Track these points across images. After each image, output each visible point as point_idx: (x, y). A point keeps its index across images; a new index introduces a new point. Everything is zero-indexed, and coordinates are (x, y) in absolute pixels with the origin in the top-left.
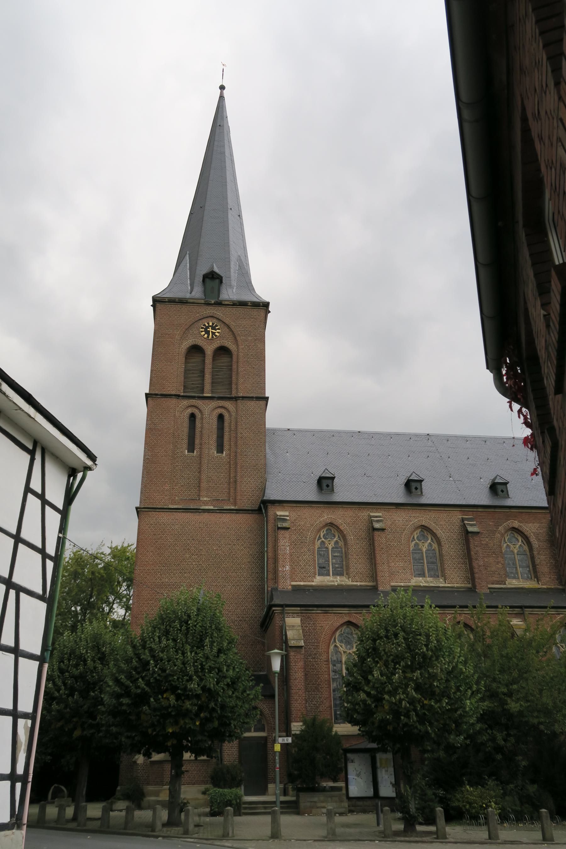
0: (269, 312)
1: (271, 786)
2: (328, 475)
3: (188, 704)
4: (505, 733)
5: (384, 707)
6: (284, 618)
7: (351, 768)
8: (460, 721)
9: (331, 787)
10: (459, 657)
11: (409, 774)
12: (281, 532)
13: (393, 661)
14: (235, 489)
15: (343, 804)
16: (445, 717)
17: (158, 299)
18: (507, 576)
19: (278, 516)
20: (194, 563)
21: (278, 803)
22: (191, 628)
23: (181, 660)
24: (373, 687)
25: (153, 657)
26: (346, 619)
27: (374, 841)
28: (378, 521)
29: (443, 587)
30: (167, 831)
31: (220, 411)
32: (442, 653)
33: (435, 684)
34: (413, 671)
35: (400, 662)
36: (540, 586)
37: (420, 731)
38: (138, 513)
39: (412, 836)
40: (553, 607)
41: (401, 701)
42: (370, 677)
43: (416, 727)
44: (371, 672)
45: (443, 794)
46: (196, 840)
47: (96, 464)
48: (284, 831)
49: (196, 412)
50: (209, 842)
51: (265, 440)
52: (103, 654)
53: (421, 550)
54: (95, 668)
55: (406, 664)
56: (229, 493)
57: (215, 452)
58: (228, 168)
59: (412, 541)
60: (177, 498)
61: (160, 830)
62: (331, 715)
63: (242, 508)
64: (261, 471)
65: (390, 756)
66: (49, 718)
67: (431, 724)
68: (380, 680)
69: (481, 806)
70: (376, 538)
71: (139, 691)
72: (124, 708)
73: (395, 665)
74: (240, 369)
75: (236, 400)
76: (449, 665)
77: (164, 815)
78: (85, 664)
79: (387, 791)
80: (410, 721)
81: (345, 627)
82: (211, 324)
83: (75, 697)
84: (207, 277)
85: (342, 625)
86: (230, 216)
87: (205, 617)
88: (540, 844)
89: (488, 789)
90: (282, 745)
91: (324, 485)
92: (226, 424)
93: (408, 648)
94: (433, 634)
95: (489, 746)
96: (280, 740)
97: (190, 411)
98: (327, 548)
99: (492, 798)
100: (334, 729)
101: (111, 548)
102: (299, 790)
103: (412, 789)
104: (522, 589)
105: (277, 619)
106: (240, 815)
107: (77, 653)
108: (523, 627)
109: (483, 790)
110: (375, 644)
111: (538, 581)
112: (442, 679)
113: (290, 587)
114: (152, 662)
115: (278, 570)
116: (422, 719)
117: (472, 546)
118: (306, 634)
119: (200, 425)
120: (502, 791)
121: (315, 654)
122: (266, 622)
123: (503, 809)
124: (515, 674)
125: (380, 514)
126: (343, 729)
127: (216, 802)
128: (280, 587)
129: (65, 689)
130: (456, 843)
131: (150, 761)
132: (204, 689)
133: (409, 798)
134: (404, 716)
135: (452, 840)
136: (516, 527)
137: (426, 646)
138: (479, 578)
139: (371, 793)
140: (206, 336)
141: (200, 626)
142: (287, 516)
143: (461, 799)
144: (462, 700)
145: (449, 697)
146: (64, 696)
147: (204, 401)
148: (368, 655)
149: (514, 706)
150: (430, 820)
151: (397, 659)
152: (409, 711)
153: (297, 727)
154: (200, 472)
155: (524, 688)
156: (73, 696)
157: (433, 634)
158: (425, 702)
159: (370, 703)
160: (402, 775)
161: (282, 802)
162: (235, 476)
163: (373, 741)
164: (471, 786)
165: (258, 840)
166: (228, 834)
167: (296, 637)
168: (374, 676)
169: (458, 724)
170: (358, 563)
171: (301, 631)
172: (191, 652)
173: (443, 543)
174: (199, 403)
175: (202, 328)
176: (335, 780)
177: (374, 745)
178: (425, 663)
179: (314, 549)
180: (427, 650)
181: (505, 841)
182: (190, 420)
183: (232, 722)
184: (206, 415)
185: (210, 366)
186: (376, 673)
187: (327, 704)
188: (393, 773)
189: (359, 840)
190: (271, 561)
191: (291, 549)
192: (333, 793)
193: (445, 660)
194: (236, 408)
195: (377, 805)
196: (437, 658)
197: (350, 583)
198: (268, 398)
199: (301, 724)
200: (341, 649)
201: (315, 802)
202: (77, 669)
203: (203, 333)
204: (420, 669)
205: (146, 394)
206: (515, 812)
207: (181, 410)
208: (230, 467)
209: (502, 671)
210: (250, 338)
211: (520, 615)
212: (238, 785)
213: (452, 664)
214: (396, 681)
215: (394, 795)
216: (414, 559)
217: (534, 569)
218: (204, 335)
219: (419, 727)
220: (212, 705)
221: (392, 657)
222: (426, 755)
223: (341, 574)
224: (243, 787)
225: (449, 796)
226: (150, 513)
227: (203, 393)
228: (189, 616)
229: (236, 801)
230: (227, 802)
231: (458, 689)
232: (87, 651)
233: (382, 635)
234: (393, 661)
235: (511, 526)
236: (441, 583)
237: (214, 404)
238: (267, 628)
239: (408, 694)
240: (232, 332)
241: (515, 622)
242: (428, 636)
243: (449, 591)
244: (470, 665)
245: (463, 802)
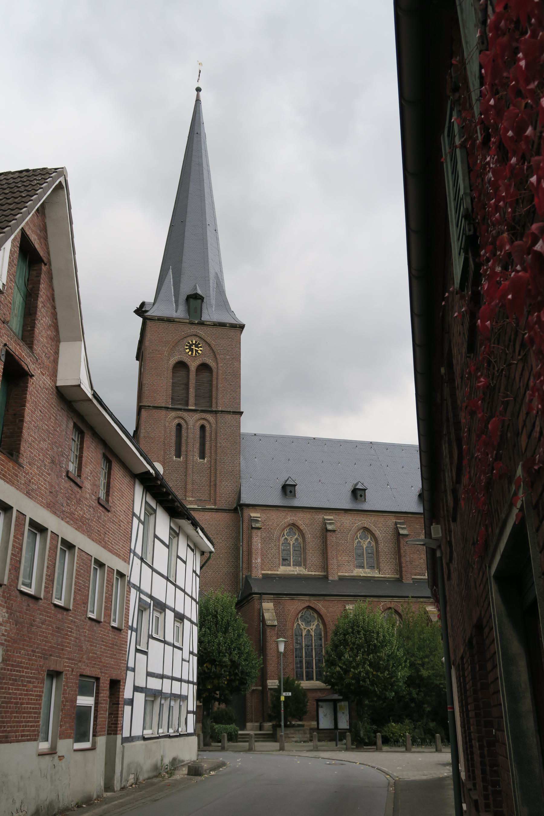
1: (249, 725)
6: (261, 603)
19: (251, 517)
24: (344, 664)
26: (307, 604)
28: (330, 524)
29: (377, 577)
31: (202, 422)
34: (368, 655)
41: (360, 672)
49: (182, 422)
53: (362, 547)
55: (365, 650)
58: (206, 181)
63: (221, 508)
64: (236, 476)
69: (400, 735)
79: (344, 724)
81: (305, 610)
82: (194, 342)
84: (191, 298)
85: (304, 609)
90: (286, 697)
92: (207, 434)
96: (284, 694)
97: (177, 421)
99: (407, 730)
106: (237, 742)
108: (435, 613)
109: (402, 725)
113: (261, 576)
115: (251, 561)
116: (373, 683)
117: (402, 545)
118: (279, 615)
119: (185, 434)
121: (284, 630)
125: (332, 517)
128: (253, 575)
132: (231, 660)
137: (377, 639)
139: (332, 727)
140: (190, 353)
142: (259, 518)
145: (389, 671)
148: (341, 643)
149: (425, 673)
151: (359, 647)
154: (186, 476)
155: (432, 661)
162: (215, 480)
164: (394, 722)
167: (271, 618)
169: (392, 685)
170: (313, 557)
174: (185, 415)
175: (187, 346)
178: (375, 650)
182: (177, 429)
184: (191, 426)
185: (194, 381)
186: (347, 656)
187: (291, 667)
190: (245, 553)
192: (299, 728)
197: (306, 572)
198: (241, 413)
200: (302, 627)
203: (188, 350)
204: (372, 653)
206: (421, 739)
208: (211, 472)
209: (420, 649)
210: (228, 357)
218: (188, 352)
223: (300, 565)
227: (187, 405)
228: (216, 611)
234: (356, 648)
236: (376, 574)
237: (197, 416)
240: (213, 350)
242: (378, 633)
243: (382, 580)
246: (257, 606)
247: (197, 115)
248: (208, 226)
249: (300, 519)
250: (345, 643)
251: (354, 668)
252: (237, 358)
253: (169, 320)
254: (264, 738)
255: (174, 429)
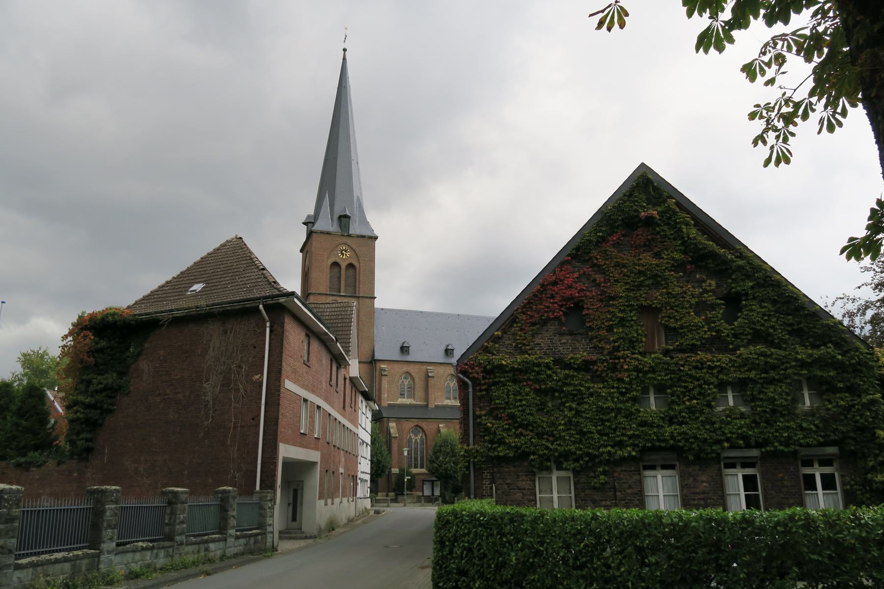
1: (380, 494)
9: (47, 560)
65: (439, 483)
79: (437, 493)
118: (399, 430)
151: (448, 454)
170: (419, 393)
227: (340, 292)
246: (386, 425)
249: (411, 369)
250: (440, 451)
252: (372, 260)
253: (328, 233)
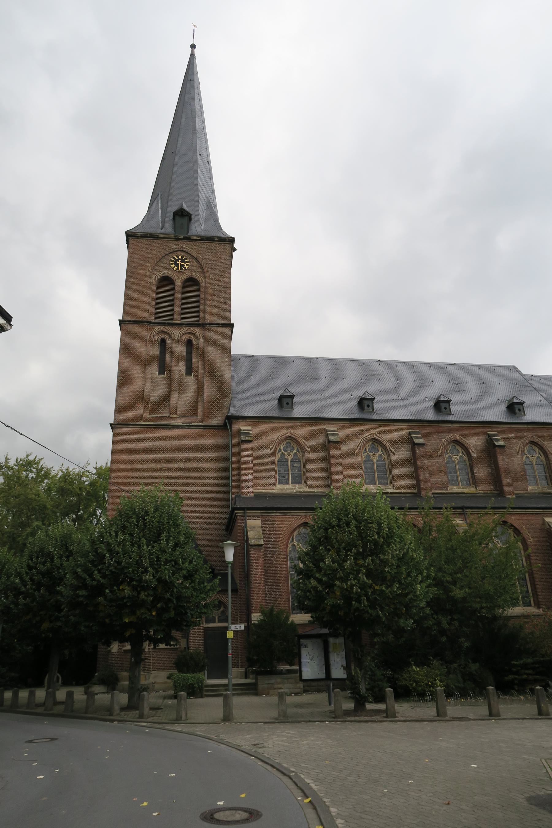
0: (235, 250)
2: (287, 394)
3: (143, 595)
4: (449, 617)
5: (335, 593)
7: (305, 653)
8: (410, 605)
9: (288, 670)
10: (410, 544)
11: (360, 657)
12: (245, 445)
13: (344, 549)
14: (203, 407)
15: (298, 685)
16: (396, 601)
17: (131, 233)
18: (448, 482)
20: (164, 474)
21: (231, 687)
22: (148, 524)
23: (137, 553)
24: (325, 575)
25: (110, 551)
26: (303, 520)
27: (325, 721)
28: (333, 435)
30: (125, 715)
31: (188, 336)
32: (393, 541)
33: (387, 570)
34: (364, 558)
35: (352, 549)
36: (478, 491)
37: (371, 615)
38: (112, 428)
39: (361, 716)
40: (492, 508)
41: (352, 586)
42: (322, 564)
43: (367, 612)
44: (323, 560)
45: (391, 674)
46: (148, 724)
47: (11, 325)
48: (236, 713)
50: (161, 726)
51: (230, 363)
52: (71, 552)
53: (372, 460)
54: (62, 565)
55: (358, 551)
56: (197, 411)
57: (184, 374)
59: (364, 453)
60: (148, 416)
61: (118, 714)
62: (289, 607)
65: (340, 640)
66: (16, 611)
67: (382, 609)
68: (331, 567)
69: (427, 684)
70: (332, 450)
71: (95, 583)
72: (81, 599)
73: (346, 553)
74: (207, 299)
75: (204, 327)
76: (400, 552)
77: (123, 698)
78: (52, 561)
79: (338, 672)
80: (361, 605)
82: (180, 257)
83: (41, 592)
84: (177, 215)
85: (299, 526)
86: (199, 161)
87: (162, 513)
88: (487, 719)
89: (433, 669)
91: (285, 404)
92: (194, 349)
93: (360, 536)
94: (385, 522)
95: (435, 630)
96: (233, 627)
97: (160, 336)
98: (287, 459)
99: (437, 676)
100: (291, 619)
101: (96, 468)
102: (258, 673)
103: (363, 671)
104: (462, 494)
105: (239, 522)
106: (202, 697)
107: (46, 550)
109: (429, 669)
110: (327, 533)
111: (476, 487)
112: (393, 565)
113: (252, 494)
114: (107, 555)
116: (373, 604)
117: (418, 456)
119: (170, 349)
120: (446, 670)
122: (230, 527)
123: (447, 686)
124: (460, 564)
125: (335, 429)
126: (301, 618)
127: (179, 686)
128: (243, 494)
129: (31, 584)
130: (405, 721)
131: (124, 650)
132: (159, 580)
133: (360, 680)
134: (356, 601)
135: (402, 719)
136: (458, 439)
137: (378, 533)
138: (424, 485)
139: (323, 676)
140: (176, 268)
141: (158, 522)
142: (250, 430)
143: (408, 679)
144: (413, 585)
145: (400, 583)
146: (31, 591)
147: (173, 327)
149: (458, 593)
150: (380, 698)
151: (350, 546)
152: (360, 596)
153: (256, 617)
154: (170, 392)
156: (39, 590)
157: (385, 522)
158: (377, 588)
159: (321, 589)
160: (353, 659)
161: (234, 685)
163: (325, 627)
164: (417, 666)
165: (209, 723)
166: (181, 718)
168: (325, 563)
169: (408, 607)
170: (315, 472)
171: (261, 531)
172: (148, 546)
173: (392, 454)
174: (169, 329)
175: (172, 261)
176: (291, 664)
177: (325, 631)
179: (274, 460)
180: (379, 537)
181: (453, 718)
182: (161, 345)
183: (188, 611)
185: (180, 296)
186: (328, 561)
188: (344, 656)
189: (309, 721)
191: (253, 460)
192: (289, 676)
193: (396, 546)
194: (204, 334)
195: (328, 686)
196: (388, 545)
197: (308, 490)
198: (233, 325)
199: (260, 614)
201: (273, 684)
202: (44, 566)
203: (173, 265)
205: (120, 321)
207: (153, 335)
208: (198, 387)
210: (217, 270)
211: (463, 515)
212: (201, 670)
213: (403, 550)
214: (347, 568)
215: (345, 676)
216: (366, 469)
217: (472, 477)
218: (174, 267)
219: (370, 611)
220: (168, 596)
221: (344, 544)
222: (375, 640)
223: (300, 483)
224: (206, 672)
225: (396, 676)
226: (124, 429)
227: (173, 320)
229: (198, 685)
230: (189, 685)
231: (409, 574)
232: (55, 549)
233: (334, 524)
234: (344, 549)
235: (453, 439)
237: (183, 330)
238: (231, 531)
239: (359, 580)
241: (458, 521)
242: (379, 524)
244: (420, 552)
245: (410, 681)
247: (191, 66)
248: (198, 156)
249: (297, 431)
251: (342, 580)
254: (242, 690)
255: (158, 345)
